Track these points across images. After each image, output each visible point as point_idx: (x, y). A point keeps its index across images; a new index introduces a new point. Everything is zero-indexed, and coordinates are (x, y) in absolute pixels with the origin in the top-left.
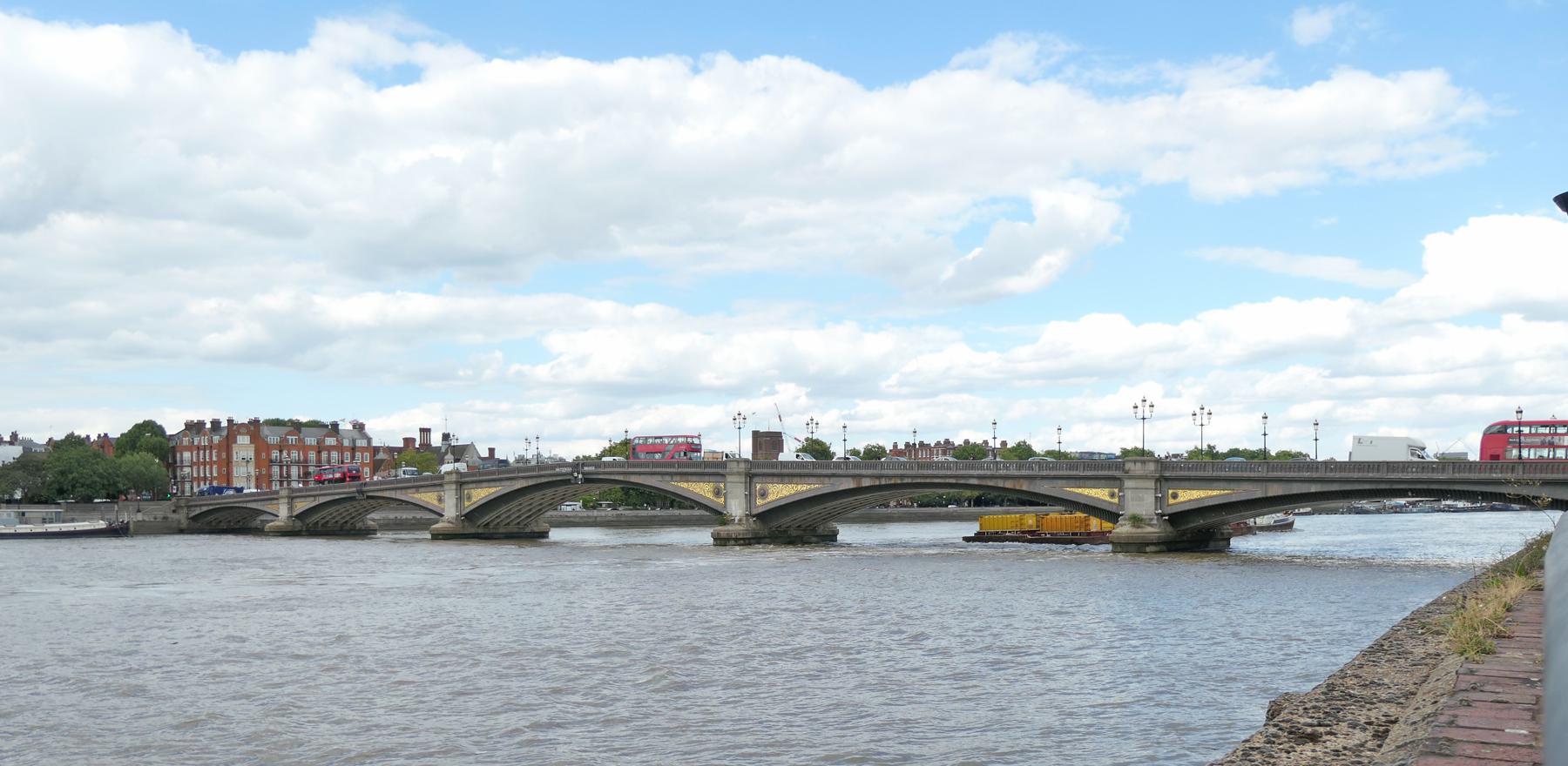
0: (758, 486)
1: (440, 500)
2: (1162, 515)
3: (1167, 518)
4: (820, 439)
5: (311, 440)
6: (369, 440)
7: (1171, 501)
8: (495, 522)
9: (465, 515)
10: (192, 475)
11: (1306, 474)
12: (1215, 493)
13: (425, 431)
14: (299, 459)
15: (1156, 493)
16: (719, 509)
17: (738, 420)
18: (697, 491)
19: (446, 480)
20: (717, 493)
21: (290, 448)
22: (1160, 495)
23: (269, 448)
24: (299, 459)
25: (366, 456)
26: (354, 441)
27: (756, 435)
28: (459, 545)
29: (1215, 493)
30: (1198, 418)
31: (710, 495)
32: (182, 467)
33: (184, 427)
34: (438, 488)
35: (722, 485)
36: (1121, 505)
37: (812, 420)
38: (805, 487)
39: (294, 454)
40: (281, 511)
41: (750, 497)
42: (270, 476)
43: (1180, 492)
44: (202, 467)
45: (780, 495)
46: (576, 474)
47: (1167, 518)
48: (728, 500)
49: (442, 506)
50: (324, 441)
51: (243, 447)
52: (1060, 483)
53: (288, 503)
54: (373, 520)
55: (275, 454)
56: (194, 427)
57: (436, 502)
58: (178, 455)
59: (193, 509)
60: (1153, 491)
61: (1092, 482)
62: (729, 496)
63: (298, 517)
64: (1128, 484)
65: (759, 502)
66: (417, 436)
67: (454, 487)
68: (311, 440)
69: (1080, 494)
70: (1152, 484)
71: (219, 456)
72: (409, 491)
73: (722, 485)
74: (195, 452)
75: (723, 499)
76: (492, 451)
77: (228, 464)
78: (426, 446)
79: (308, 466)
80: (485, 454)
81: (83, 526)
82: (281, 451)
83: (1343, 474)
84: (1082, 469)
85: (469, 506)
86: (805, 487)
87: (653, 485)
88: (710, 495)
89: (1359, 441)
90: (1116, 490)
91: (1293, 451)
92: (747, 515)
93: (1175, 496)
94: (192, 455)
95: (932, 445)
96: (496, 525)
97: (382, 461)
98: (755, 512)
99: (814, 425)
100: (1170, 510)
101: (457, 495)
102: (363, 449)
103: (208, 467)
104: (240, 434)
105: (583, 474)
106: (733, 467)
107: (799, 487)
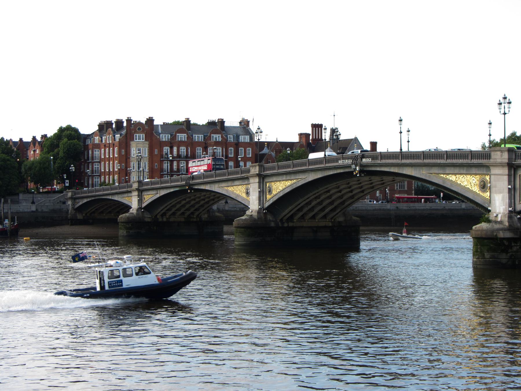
1: (248, 193)
5: (198, 137)
10: (100, 170)
16: (486, 205)
17: (503, 105)
18: (465, 184)
19: (251, 173)
20: (483, 186)
23: (162, 144)
26: (238, 137)
31: (476, 189)
32: (93, 163)
33: (97, 128)
37: (505, 98)
39: (183, 149)
45: (278, 191)
50: (176, 135)
53: (138, 196)
55: (166, 149)
56: (104, 127)
57: (244, 195)
58: (90, 153)
59: (77, 201)
61: (457, 170)
62: (493, 189)
66: (309, 131)
68: (198, 137)
71: (119, 152)
72: (448, 170)
73: (487, 178)
74: (103, 150)
75: (488, 194)
76: (374, 145)
77: (126, 159)
80: (367, 147)
82: (171, 148)
86: (288, 183)
87: (424, 177)
88: (476, 189)
91: (198, 124)
92: (510, 211)
97: (264, 155)
101: (259, 188)
102: (246, 145)
104: (136, 132)
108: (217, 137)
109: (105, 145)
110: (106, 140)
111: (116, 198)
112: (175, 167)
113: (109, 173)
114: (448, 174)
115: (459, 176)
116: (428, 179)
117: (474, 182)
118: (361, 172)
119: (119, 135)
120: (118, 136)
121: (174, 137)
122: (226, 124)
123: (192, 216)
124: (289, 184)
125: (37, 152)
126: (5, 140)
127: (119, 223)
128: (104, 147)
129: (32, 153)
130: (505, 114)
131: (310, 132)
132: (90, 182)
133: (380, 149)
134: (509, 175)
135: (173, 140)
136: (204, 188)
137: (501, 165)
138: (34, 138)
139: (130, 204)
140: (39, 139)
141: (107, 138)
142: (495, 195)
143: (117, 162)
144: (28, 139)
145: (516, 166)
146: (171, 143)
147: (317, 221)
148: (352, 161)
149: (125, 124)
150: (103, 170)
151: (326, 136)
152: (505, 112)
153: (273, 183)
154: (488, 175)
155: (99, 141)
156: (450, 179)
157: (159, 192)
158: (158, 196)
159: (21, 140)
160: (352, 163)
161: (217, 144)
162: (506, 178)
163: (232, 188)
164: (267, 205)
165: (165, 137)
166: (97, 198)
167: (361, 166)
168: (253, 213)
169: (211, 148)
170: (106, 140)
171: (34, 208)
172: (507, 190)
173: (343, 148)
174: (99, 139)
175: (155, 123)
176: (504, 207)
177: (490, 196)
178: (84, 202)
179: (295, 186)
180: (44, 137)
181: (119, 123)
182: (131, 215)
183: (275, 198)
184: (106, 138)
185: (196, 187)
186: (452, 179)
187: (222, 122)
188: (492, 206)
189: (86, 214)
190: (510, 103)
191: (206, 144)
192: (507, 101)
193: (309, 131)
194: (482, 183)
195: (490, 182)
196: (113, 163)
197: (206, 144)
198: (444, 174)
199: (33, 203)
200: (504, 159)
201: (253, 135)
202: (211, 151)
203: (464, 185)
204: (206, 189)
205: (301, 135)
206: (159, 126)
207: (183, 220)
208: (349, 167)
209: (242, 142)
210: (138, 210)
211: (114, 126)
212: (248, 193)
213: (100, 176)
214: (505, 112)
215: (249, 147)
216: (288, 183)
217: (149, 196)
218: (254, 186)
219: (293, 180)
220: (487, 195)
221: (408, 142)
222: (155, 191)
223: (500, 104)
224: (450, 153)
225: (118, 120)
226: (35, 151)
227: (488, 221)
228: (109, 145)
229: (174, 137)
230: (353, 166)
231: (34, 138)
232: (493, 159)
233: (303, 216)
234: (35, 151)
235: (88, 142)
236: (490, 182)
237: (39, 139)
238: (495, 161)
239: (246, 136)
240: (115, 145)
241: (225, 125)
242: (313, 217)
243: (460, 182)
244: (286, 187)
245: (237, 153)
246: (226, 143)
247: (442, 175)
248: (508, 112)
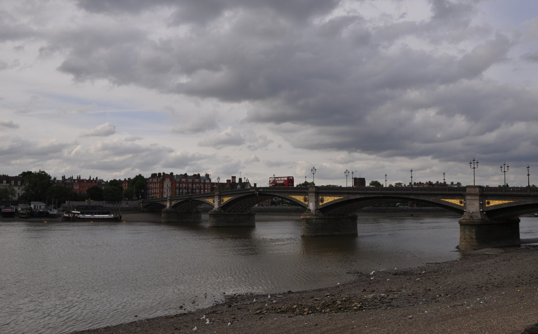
0: (320, 197)
1: (214, 202)
2: (483, 212)
3: (485, 213)
4: (467, 185)
5: (190, 180)
6: (210, 180)
7: (487, 205)
9: (221, 207)
11: (424, 192)
12: (506, 202)
14: (186, 187)
15: (480, 201)
17: (313, 171)
18: (298, 199)
19: (215, 194)
20: (305, 200)
21: (183, 183)
22: (482, 203)
23: (176, 182)
24: (186, 187)
25: (209, 186)
26: (205, 180)
27: (355, 180)
29: (506, 202)
30: (472, 165)
31: (303, 201)
35: (307, 197)
36: (465, 207)
39: (184, 185)
40: (167, 205)
41: (317, 202)
42: (176, 192)
43: (491, 201)
44: (155, 189)
45: (328, 201)
46: (256, 192)
47: (485, 213)
51: (167, 183)
54: (200, 208)
56: (154, 175)
57: (212, 202)
58: (148, 185)
60: (478, 201)
62: (309, 201)
64: (468, 197)
65: (321, 204)
66: (231, 179)
67: (218, 197)
68: (190, 180)
69: (450, 203)
70: (478, 198)
71: (160, 186)
73: (307, 197)
75: (307, 203)
76: (255, 184)
78: (234, 182)
80: (253, 185)
82: (180, 184)
83: (406, 191)
84: (448, 191)
85: (322, 205)
86: (230, 198)
88: (303, 201)
90: (463, 200)
92: (315, 209)
93: (489, 203)
94: (186, 185)
95: (425, 183)
97: (215, 187)
98: (318, 208)
100: (486, 210)
102: (208, 184)
103: (156, 189)
106: (311, 189)
107: (335, 198)
108: (197, 180)
110: (154, 181)
111: (160, 203)
112: (181, 192)
114: (292, 195)
118: (258, 194)
121: (181, 180)
122: (201, 176)
125: (126, 185)
126: (502, 186)
129: (124, 185)
130: (347, 176)
131: (231, 179)
132: (148, 197)
133: (258, 186)
134: (315, 196)
136: (423, 199)
137: (312, 192)
138: (125, 179)
139: (166, 205)
140: (127, 179)
141: (155, 180)
144: (123, 179)
149: (162, 175)
150: (153, 192)
151: (237, 181)
152: (528, 174)
154: (307, 196)
158: (177, 202)
159: (120, 180)
162: (314, 197)
164: (221, 206)
165: (178, 180)
167: (259, 192)
170: (154, 181)
171: (127, 206)
172: (314, 202)
175: (174, 174)
179: (232, 199)
180: (129, 179)
181: (160, 174)
185: (193, 199)
187: (199, 175)
190: (315, 170)
192: (315, 169)
193: (231, 179)
195: (308, 198)
196: (157, 190)
199: (127, 204)
204: (426, 200)
205: (227, 180)
208: (254, 192)
210: (169, 207)
211: (158, 175)
212: (214, 202)
213: (152, 194)
214: (528, 174)
216: (230, 198)
220: (307, 203)
223: (345, 172)
224: (453, 188)
225: (159, 173)
226: (125, 184)
229: (181, 180)
230: (256, 192)
231: (125, 179)
233: (234, 210)
234: (125, 184)
235: (147, 181)
236: (308, 198)
237: (127, 179)
242: (238, 211)
245: (204, 186)
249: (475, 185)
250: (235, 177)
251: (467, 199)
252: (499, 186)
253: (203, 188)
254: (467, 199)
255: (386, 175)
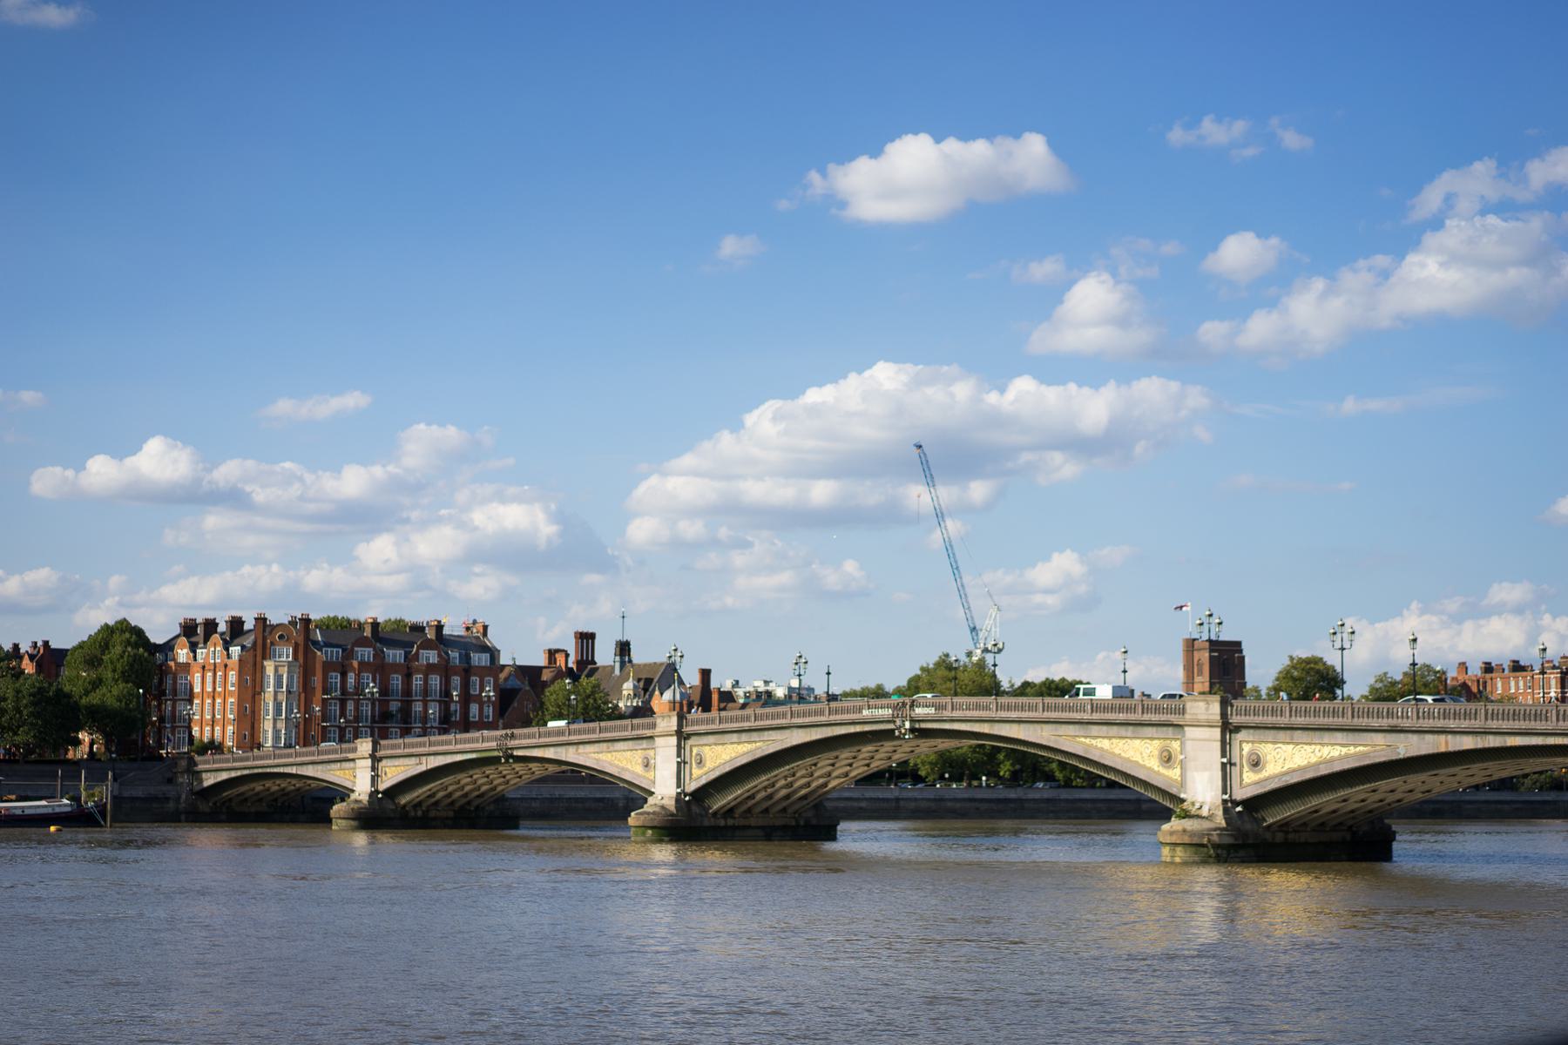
0: (1247, 748)
8: (744, 807)
13: (586, 639)
16: (1174, 791)
17: (1339, 636)
20: (1167, 759)
28: (409, 839)
31: (1154, 764)
34: (644, 744)
38: (1336, 752)
45: (718, 762)
48: (1189, 775)
49: (650, 775)
50: (352, 650)
52: (1071, 729)
57: (639, 769)
62: (1190, 765)
63: (388, 792)
65: (1249, 777)
66: (571, 646)
68: (395, 655)
73: (1176, 745)
76: (706, 674)
79: (388, 701)
81: (39, 807)
88: (1154, 764)
89: (302, 615)
96: (745, 812)
99: (1345, 636)
105: (912, 721)
109: (204, 667)
113: (213, 722)
115: (1118, 741)
116: (1051, 745)
117: (1148, 752)
119: (239, 648)
120: (235, 650)
123: (468, 808)
124: (745, 749)
127: (334, 820)
128: (201, 670)
135: (347, 659)
142: (1195, 774)
143: (233, 700)
145: (1235, 727)
146: (343, 666)
147: (771, 816)
148: (893, 712)
152: (1414, 661)
153: (707, 748)
154: (1176, 739)
155: (188, 658)
156: (1099, 745)
157: (424, 762)
158: (423, 768)
160: (893, 715)
161: (431, 668)
163: (609, 755)
166: (256, 771)
167: (912, 721)
168: (663, 802)
169: (418, 676)
173: (646, 679)
174: (187, 654)
176: (1213, 793)
177: (1182, 775)
178: (219, 779)
179: (759, 754)
182: (356, 806)
183: (713, 776)
184: (208, 654)
186: (1103, 746)
188: (1188, 791)
189: (215, 804)
191: (408, 668)
194: (1165, 754)
197: (408, 668)
198: (1086, 737)
200: (1215, 714)
201: (496, 653)
202: (418, 682)
203: (1127, 756)
206: (501, 726)
207: (451, 814)
209: (476, 667)
214: (1414, 661)
215: (489, 676)
217: (398, 768)
218: (665, 750)
219: (755, 742)
221: (828, 673)
222: (413, 759)
224: (1103, 702)
227: (1186, 815)
228: (215, 667)
231: (16, 647)
232: (1190, 714)
238: (1195, 717)
239: (484, 655)
240: (230, 666)
241: (444, 633)
243: (1120, 752)
244: (738, 755)
246: (446, 667)
247: (1083, 739)
248: (1349, 647)
249: (803, 685)
250: (592, 636)
251: (1193, 740)
252: (922, 669)
253: (231, 673)
254: (1193, 740)
255: (1415, 640)
